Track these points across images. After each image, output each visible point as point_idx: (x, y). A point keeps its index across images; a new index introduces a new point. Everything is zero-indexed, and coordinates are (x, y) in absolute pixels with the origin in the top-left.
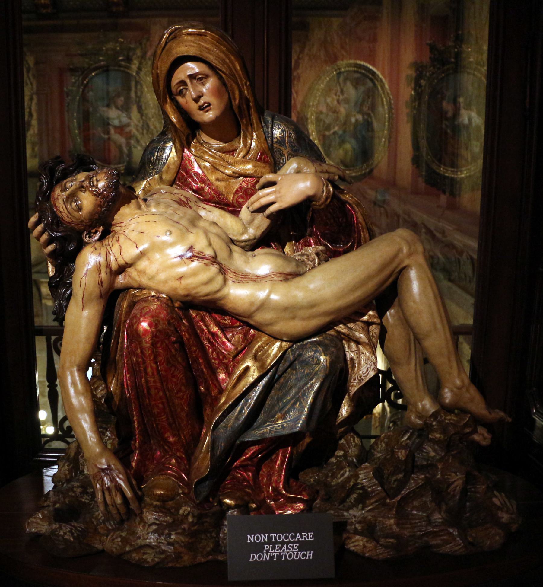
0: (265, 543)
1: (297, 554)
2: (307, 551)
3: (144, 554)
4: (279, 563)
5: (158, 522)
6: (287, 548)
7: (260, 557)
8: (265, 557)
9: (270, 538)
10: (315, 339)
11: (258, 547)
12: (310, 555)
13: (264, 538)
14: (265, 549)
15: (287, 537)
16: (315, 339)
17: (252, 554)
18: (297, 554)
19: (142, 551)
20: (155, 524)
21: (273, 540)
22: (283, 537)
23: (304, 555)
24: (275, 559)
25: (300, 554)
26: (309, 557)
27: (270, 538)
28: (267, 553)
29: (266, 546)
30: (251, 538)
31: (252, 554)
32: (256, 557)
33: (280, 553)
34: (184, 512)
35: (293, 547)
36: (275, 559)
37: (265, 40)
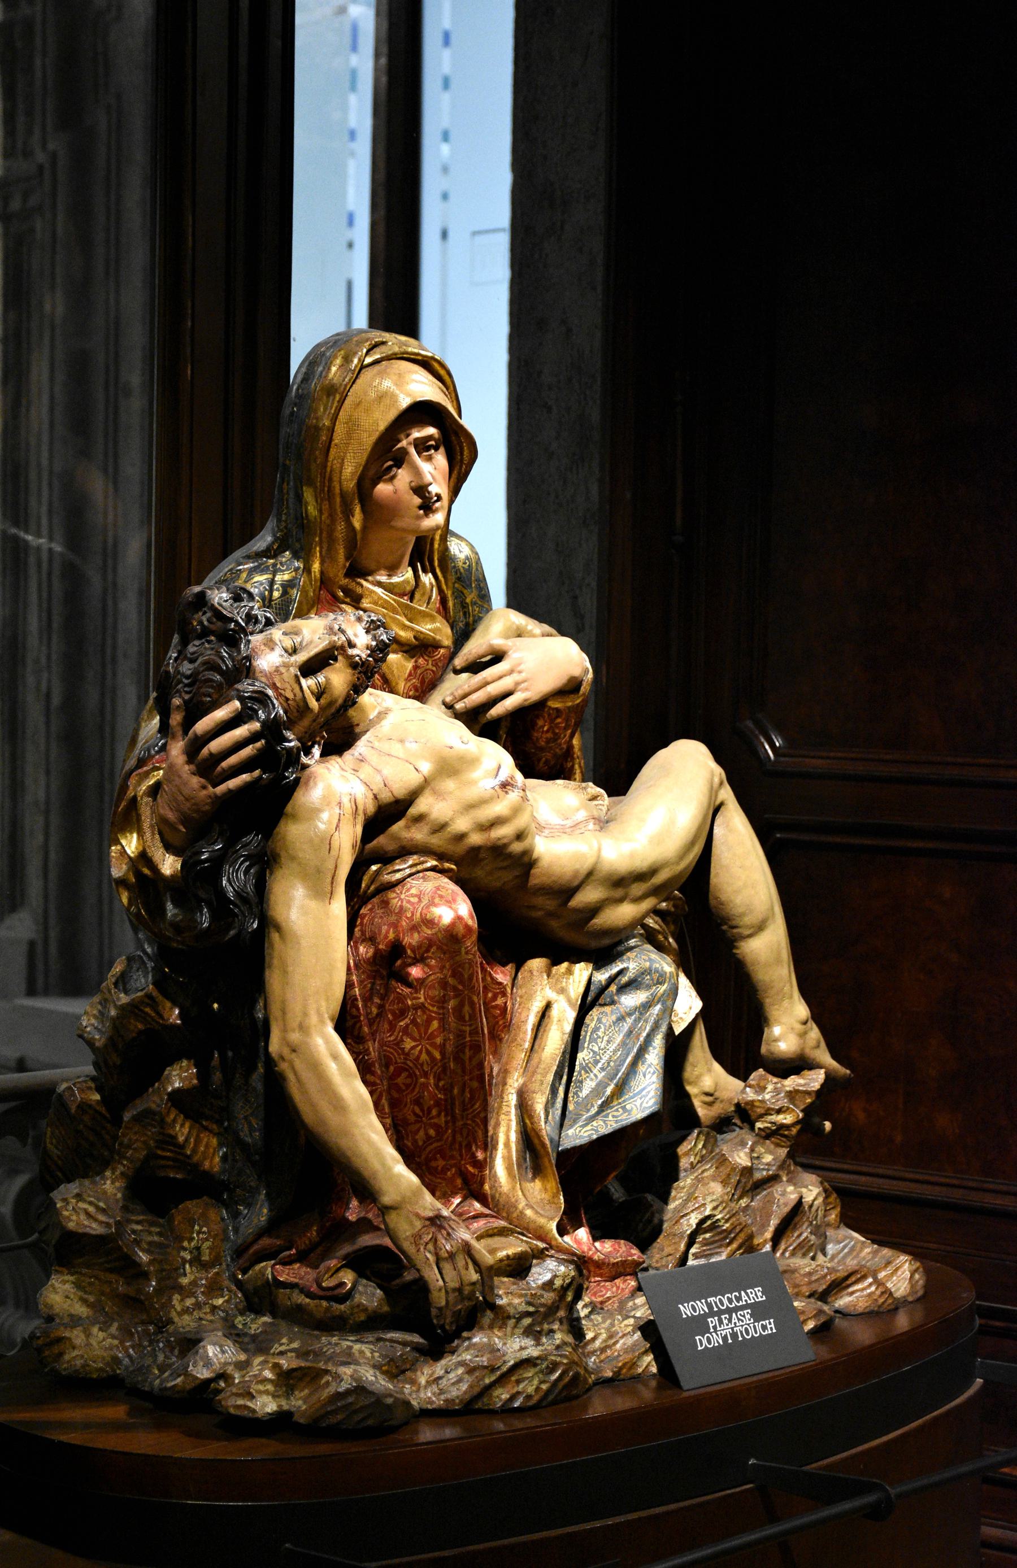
0: (706, 1316)
1: (754, 1327)
2: (764, 1320)
3: (518, 1382)
4: (735, 1346)
5: (531, 1309)
6: (739, 1319)
7: (709, 1341)
8: (717, 1340)
9: (710, 1306)
10: (998, 1324)
11: (700, 1324)
12: (771, 1326)
13: (701, 1307)
14: (711, 1325)
15: (730, 1301)
16: (998, 1324)
17: (697, 1338)
18: (754, 1327)
19: (513, 1379)
20: (528, 1314)
21: (716, 1309)
22: (726, 1301)
23: (764, 1328)
24: (730, 1341)
25: (758, 1326)
26: (771, 1329)
27: (710, 1306)
28: (716, 1331)
29: (709, 1320)
30: (686, 1310)
31: (697, 1338)
32: (705, 1342)
33: (732, 1329)
34: (564, 1280)
35: (744, 1316)
36: (730, 1341)
37: (838, 840)
